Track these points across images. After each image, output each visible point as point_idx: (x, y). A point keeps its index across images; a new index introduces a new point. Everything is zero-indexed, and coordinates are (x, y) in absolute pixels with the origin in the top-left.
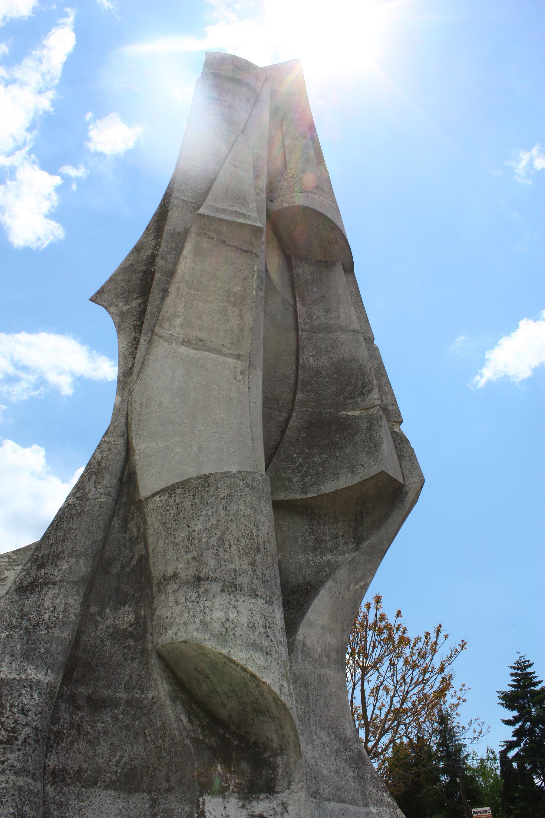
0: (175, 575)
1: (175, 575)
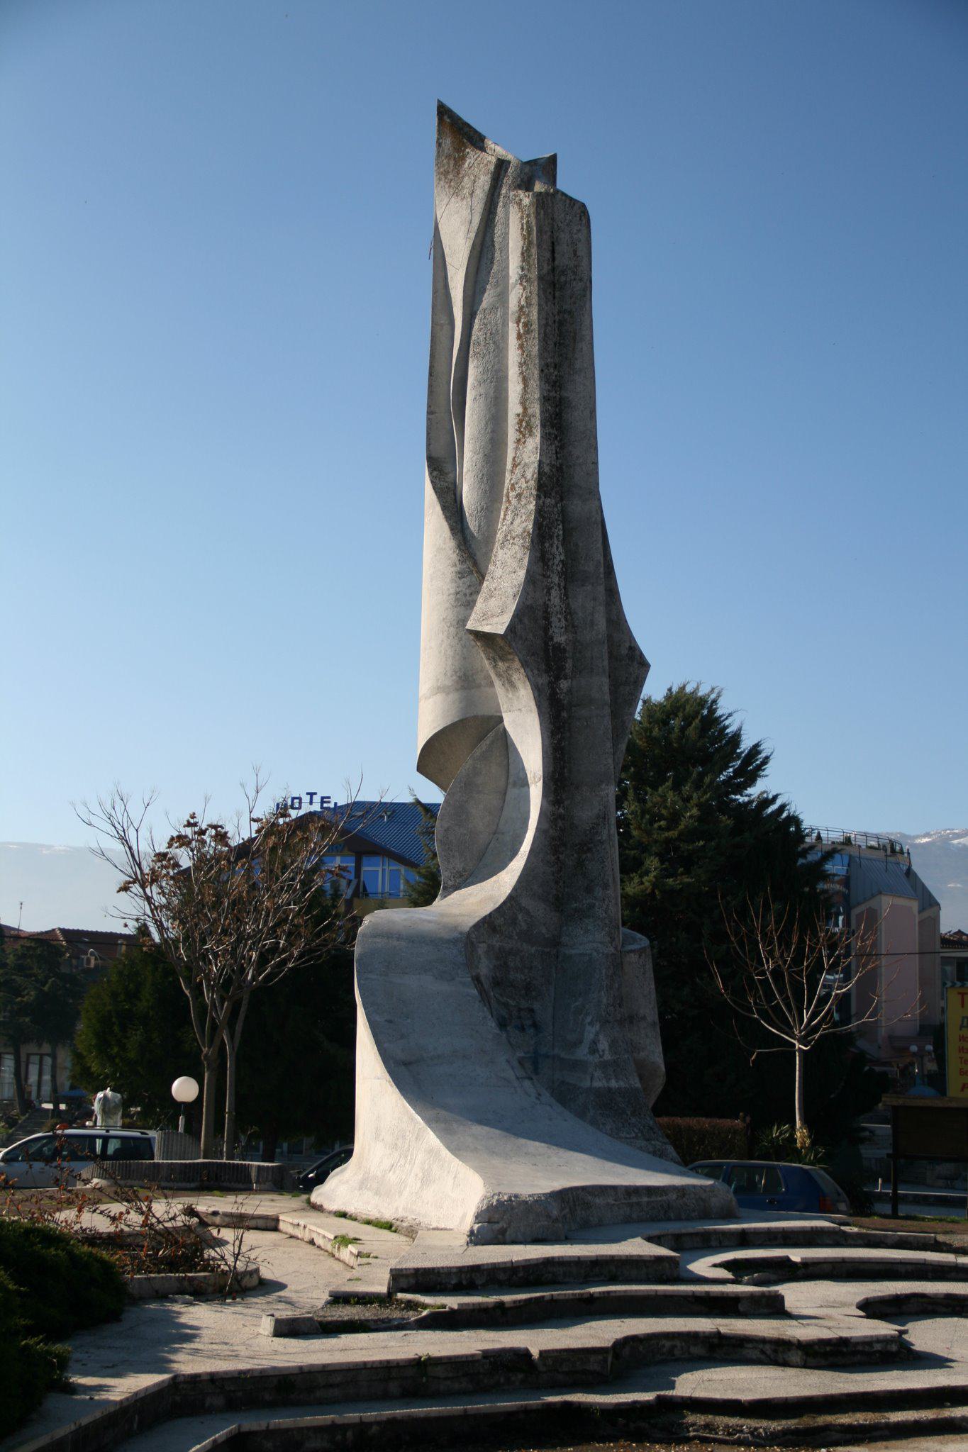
0: (644, 1018)
1: (644, 1018)
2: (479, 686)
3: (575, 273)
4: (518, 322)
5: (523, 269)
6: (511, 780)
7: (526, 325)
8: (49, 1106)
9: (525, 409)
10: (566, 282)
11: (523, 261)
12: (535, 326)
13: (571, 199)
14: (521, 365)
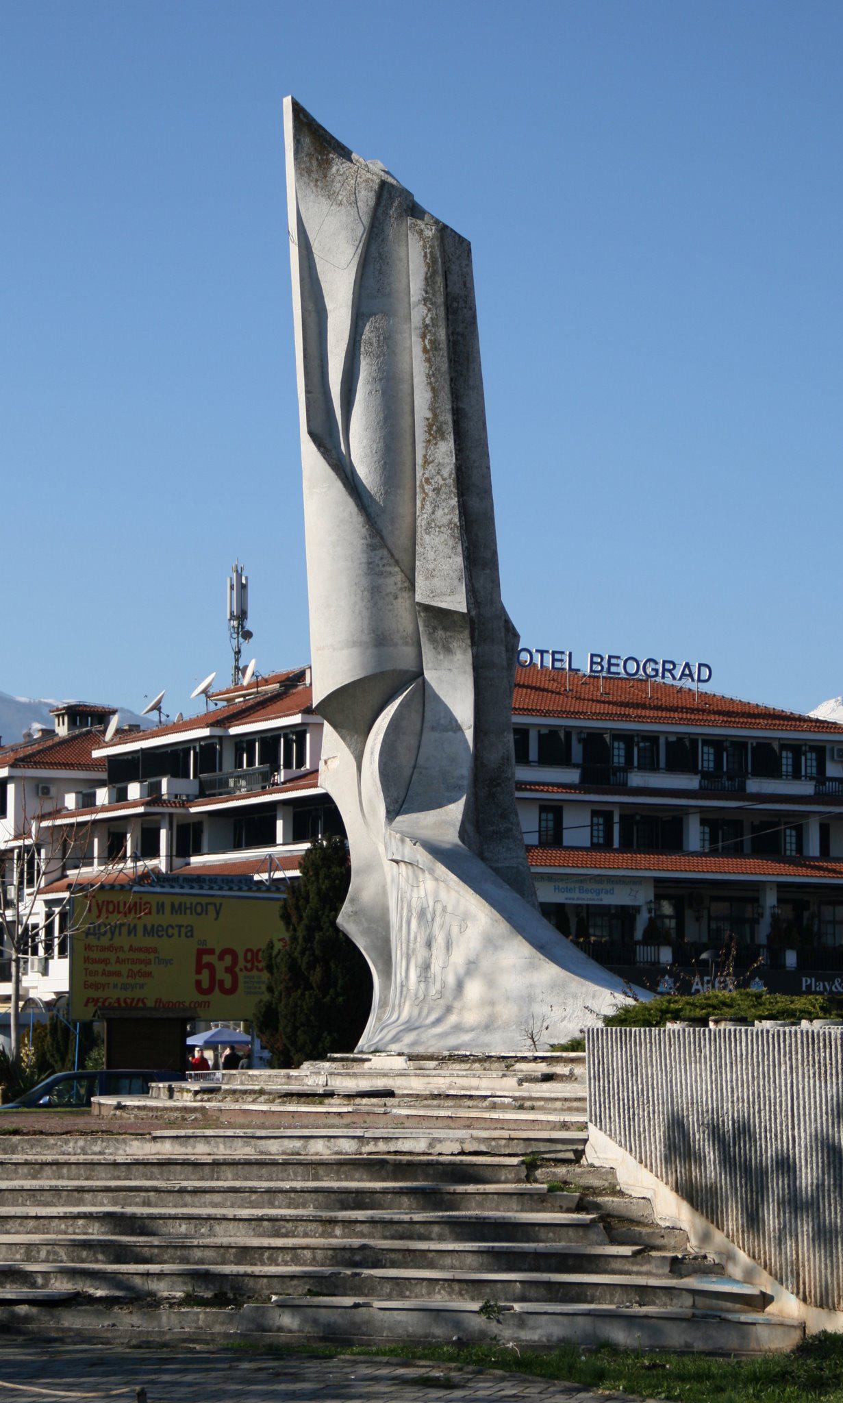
2: (396, 645)
3: (466, 302)
4: (423, 337)
5: (427, 292)
6: (427, 725)
7: (432, 342)
8: (704, 956)
9: (435, 416)
10: (458, 308)
11: (427, 284)
12: (444, 346)
13: (460, 236)
14: (428, 376)
